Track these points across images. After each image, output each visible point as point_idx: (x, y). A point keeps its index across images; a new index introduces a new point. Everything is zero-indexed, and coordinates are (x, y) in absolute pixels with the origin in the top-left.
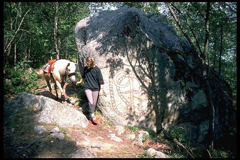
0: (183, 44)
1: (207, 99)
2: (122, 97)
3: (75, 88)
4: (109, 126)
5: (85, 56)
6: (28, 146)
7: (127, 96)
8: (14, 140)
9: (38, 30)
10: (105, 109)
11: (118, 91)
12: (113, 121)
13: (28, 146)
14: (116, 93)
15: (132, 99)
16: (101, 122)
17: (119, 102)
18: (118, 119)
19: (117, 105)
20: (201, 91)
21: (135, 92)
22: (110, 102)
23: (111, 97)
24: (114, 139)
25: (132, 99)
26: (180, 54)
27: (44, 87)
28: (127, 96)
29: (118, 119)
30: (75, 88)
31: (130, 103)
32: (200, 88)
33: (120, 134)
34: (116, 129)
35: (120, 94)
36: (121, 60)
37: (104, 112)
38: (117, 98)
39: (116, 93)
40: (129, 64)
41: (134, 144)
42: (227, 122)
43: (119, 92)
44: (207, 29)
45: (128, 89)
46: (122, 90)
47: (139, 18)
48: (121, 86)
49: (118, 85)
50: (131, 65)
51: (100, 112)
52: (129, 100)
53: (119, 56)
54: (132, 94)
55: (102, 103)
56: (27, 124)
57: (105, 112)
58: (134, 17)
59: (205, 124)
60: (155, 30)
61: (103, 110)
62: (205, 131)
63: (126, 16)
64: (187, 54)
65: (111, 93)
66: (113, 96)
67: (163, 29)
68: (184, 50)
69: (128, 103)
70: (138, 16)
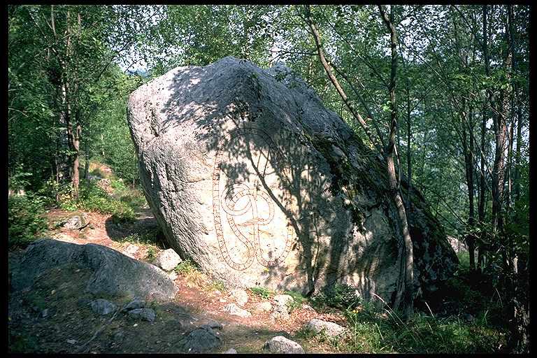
0: (336, 125)
1: (390, 226)
2: (237, 233)
3: (119, 225)
4: (218, 292)
5: (160, 159)
6: (93, 338)
7: (245, 231)
8: (56, 330)
9: (43, 109)
10: (208, 261)
11: (230, 222)
12: (224, 280)
13: (93, 338)
14: (226, 227)
15: (256, 236)
16: (200, 286)
17: (232, 245)
18: (233, 277)
19: (229, 250)
20: (380, 212)
21: (262, 223)
22: (217, 246)
23: (218, 235)
24: (236, 314)
25: (256, 236)
26: (336, 145)
27: (58, 226)
28: (245, 231)
29: (233, 277)
30: (119, 225)
31: (253, 244)
32: (377, 206)
33: (242, 304)
34: (232, 296)
35: (233, 226)
36: (244, 165)
37: (206, 265)
38: (228, 235)
39: (226, 227)
40: (256, 173)
41: (275, 319)
42: (428, 266)
43: (231, 225)
44: (403, 276)
45: (249, 217)
46: (238, 220)
47: (258, 82)
48: (236, 213)
49: (232, 213)
50: (258, 173)
51: (197, 265)
52: (251, 238)
53: (240, 158)
54: (256, 227)
55: (200, 247)
56: (72, 299)
57: (207, 266)
58: (249, 81)
59: (388, 272)
60: (288, 102)
61: (203, 261)
62: (391, 285)
63: (234, 78)
64: (347, 144)
65: (217, 228)
66: (218, 231)
67: (300, 97)
68: (341, 136)
69: (249, 245)
70: (255, 78)
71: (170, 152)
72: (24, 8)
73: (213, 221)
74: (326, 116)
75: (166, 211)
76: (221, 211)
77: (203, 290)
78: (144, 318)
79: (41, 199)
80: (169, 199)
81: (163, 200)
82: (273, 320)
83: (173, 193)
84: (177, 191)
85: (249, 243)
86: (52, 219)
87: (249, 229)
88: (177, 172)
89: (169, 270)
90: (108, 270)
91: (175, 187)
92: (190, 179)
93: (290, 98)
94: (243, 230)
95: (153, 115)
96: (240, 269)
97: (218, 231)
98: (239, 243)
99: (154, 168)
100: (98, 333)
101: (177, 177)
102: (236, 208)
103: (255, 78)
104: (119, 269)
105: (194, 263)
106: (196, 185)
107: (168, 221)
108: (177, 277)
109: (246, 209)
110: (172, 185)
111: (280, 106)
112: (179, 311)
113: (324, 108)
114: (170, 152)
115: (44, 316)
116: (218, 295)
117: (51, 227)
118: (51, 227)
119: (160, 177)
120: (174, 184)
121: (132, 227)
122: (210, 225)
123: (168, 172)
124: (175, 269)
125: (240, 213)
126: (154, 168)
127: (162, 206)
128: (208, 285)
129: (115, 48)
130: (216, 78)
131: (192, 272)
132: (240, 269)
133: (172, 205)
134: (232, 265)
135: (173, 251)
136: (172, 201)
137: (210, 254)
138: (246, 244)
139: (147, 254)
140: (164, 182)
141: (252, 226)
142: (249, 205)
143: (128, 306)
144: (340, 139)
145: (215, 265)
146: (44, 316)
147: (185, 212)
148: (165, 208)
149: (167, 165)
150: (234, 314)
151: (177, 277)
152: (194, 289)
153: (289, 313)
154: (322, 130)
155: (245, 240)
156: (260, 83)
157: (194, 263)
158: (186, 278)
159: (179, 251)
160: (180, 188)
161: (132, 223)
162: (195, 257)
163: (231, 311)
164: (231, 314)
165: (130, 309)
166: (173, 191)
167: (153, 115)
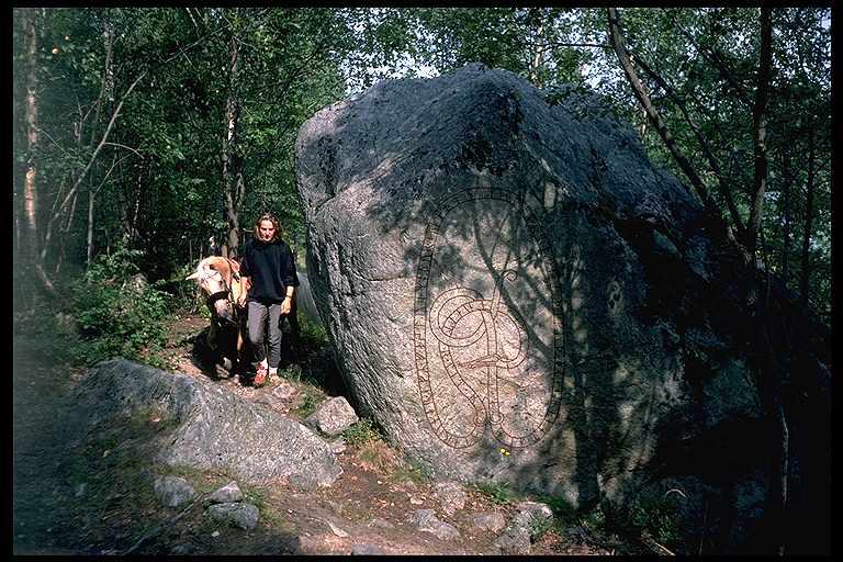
5: (331, 236)
16: (383, 469)
26: (664, 232)
36: (454, 250)
47: (517, 105)
53: (448, 235)
58: (502, 103)
60: (575, 148)
67: (601, 141)
70: (514, 98)
71: (346, 225)
72: (620, 249)
75: (336, 330)
81: (334, 309)
83: (348, 299)
84: (353, 294)
86: (179, 330)
88: (356, 260)
90: (200, 425)
91: (352, 287)
92: (376, 273)
93: (582, 141)
94: (466, 374)
95: (332, 159)
99: (322, 252)
101: (355, 270)
104: (227, 425)
105: (378, 427)
107: (340, 346)
110: (348, 284)
111: (557, 153)
113: (649, 165)
114: (346, 225)
115: (78, 494)
116: (409, 490)
117: (172, 342)
118: (172, 342)
119: (331, 269)
120: (350, 282)
123: (342, 261)
124: (345, 434)
126: (322, 252)
127: (332, 319)
128: (396, 468)
129: (385, 112)
130: (444, 98)
131: (373, 443)
133: (344, 319)
135: (344, 400)
137: (405, 413)
139: (303, 403)
141: (485, 369)
143: (213, 497)
145: (411, 432)
146: (78, 494)
147: (365, 333)
148: (336, 325)
149: (340, 247)
152: (369, 474)
156: (522, 108)
157: (378, 427)
159: (355, 403)
160: (359, 288)
162: (380, 416)
165: (214, 502)
166: (348, 295)
167: (332, 159)
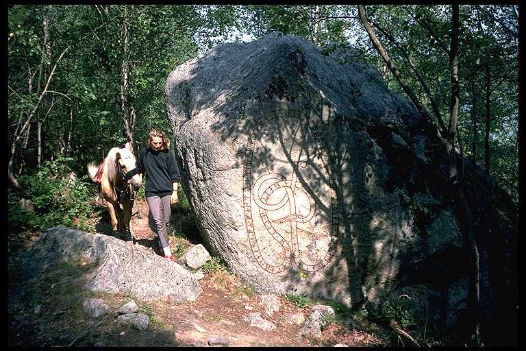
2: (271, 231)
4: (245, 297)
10: (237, 260)
14: (258, 221)
16: (228, 288)
21: (301, 220)
23: (249, 232)
31: (290, 244)
33: (270, 313)
35: (268, 223)
36: (267, 150)
39: (258, 221)
41: (303, 336)
45: (285, 212)
47: (303, 57)
48: (269, 207)
51: (226, 265)
53: (263, 140)
55: (229, 245)
58: (293, 56)
59: (457, 285)
60: (340, 82)
61: (232, 261)
63: (275, 53)
66: (249, 228)
67: (357, 78)
70: (300, 53)
71: (198, 137)
73: (243, 216)
74: (389, 99)
75: (195, 203)
76: (253, 205)
77: (229, 293)
78: (133, 325)
79: (84, 186)
80: (198, 190)
81: (193, 190)
82: (300, 337)
83: (202, 183)
84: (204, 180)
85: (285, 243)
87: (286, 226)
88: (205, 160)
89: (195, 267)
91: (204, 176)
96: (274, 272)
97: (249, 228)
98: (274, 243)
100: (77, 340)
102: (270, 201)
103: (300, 53)
105: (223, 262)
106: (225, 174)
108: (203, 276)
109: (283, 203)
110: (201, 173)
112: (149, 329)
116: (244, 301)
119: (190, 165)
121: (184, 218)
122: (239, 218)
123: (197, 159)
125: (276, 207)
126: (185, 154)
128: (236, 287)
131: (221, 272)
132: (274, 272)
133: (200, 196)
134: (264, 267)
136: (200, 192)
137: (239, 253)
138: (281, 243)
139: (176, 249)
140: (193, 170)
141: (289, 223)
142: (286, 199)
144: (405, 127)
145: (245, 265)
147: (213, 204)
148: (194, 199)
150: (255, 325)
151: (203, 276)
152: (219, 292)
153: (322, 329)
154: (382, 114)
155: (280, 239)
157: (223, 262)
158: (214, 278)
160: (208, 176)
161: (186, 214)
162: (224, 255)
163: (252, 322)
164: (252, 325)
165: (120, 314)
166: (201, 180)
